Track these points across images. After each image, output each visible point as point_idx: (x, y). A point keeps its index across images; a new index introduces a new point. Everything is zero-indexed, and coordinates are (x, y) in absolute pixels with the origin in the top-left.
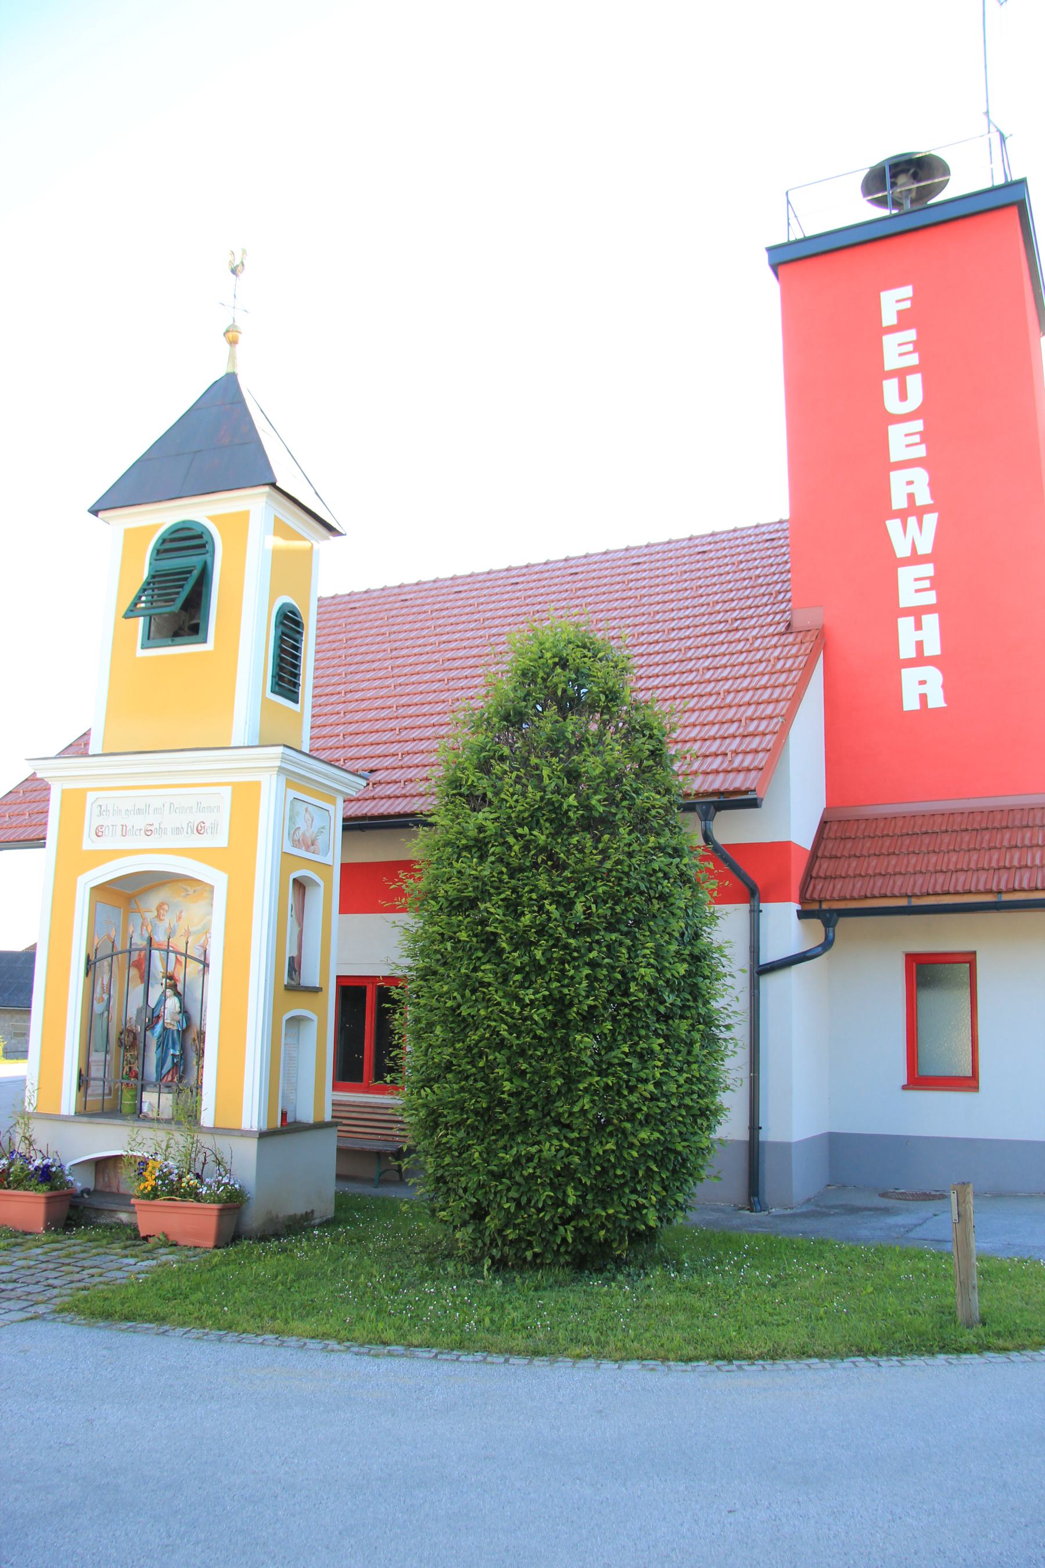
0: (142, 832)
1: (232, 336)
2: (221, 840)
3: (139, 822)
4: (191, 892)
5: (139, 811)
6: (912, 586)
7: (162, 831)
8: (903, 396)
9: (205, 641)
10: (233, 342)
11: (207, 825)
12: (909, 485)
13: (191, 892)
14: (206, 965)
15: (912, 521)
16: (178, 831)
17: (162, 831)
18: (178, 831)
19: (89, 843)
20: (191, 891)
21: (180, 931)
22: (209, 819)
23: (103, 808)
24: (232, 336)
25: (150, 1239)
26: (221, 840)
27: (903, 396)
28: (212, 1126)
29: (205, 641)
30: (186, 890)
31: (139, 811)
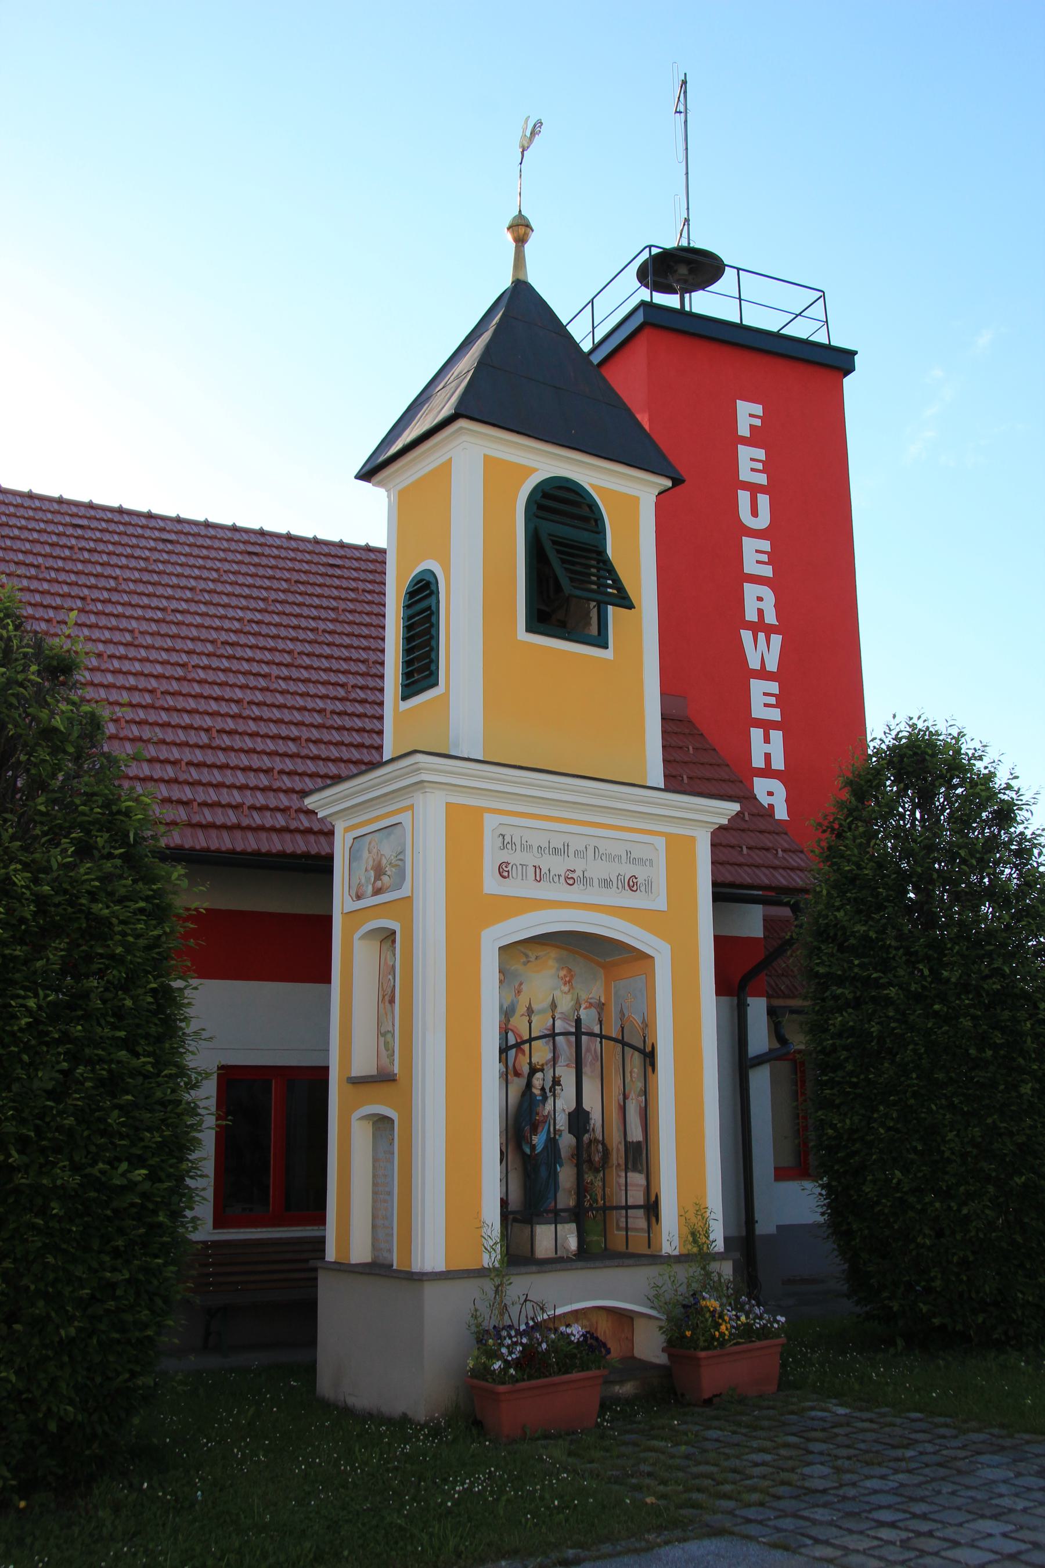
0: (562, 879)
1: (521, 229)
2: (659, 902)
3: (558, 865)
4: (532, 959)
5: (556, 851)
6: (762, 698)
7: (586, 881)
8: (755, 513)
9: (529, 629)
10: (520, 241)
11: (640, 880)
12: (759, 601)
13: (532, 959)
14: (650, 1057)
15: (761, 636)
16: (606, 883)
17: (586, 881)
18: (606, 883)
19: (491, 884)
20: (532, 956)
21: (522, 1009)
22: (641, 873)
23: (508, 839)
24: (521, 229)
25: (715, 1400)
26: (659, 902)
27: (755, 513)
28: (369, 1260)
29: (529, 629)
30: (527, 956)
31: (556, 851)
